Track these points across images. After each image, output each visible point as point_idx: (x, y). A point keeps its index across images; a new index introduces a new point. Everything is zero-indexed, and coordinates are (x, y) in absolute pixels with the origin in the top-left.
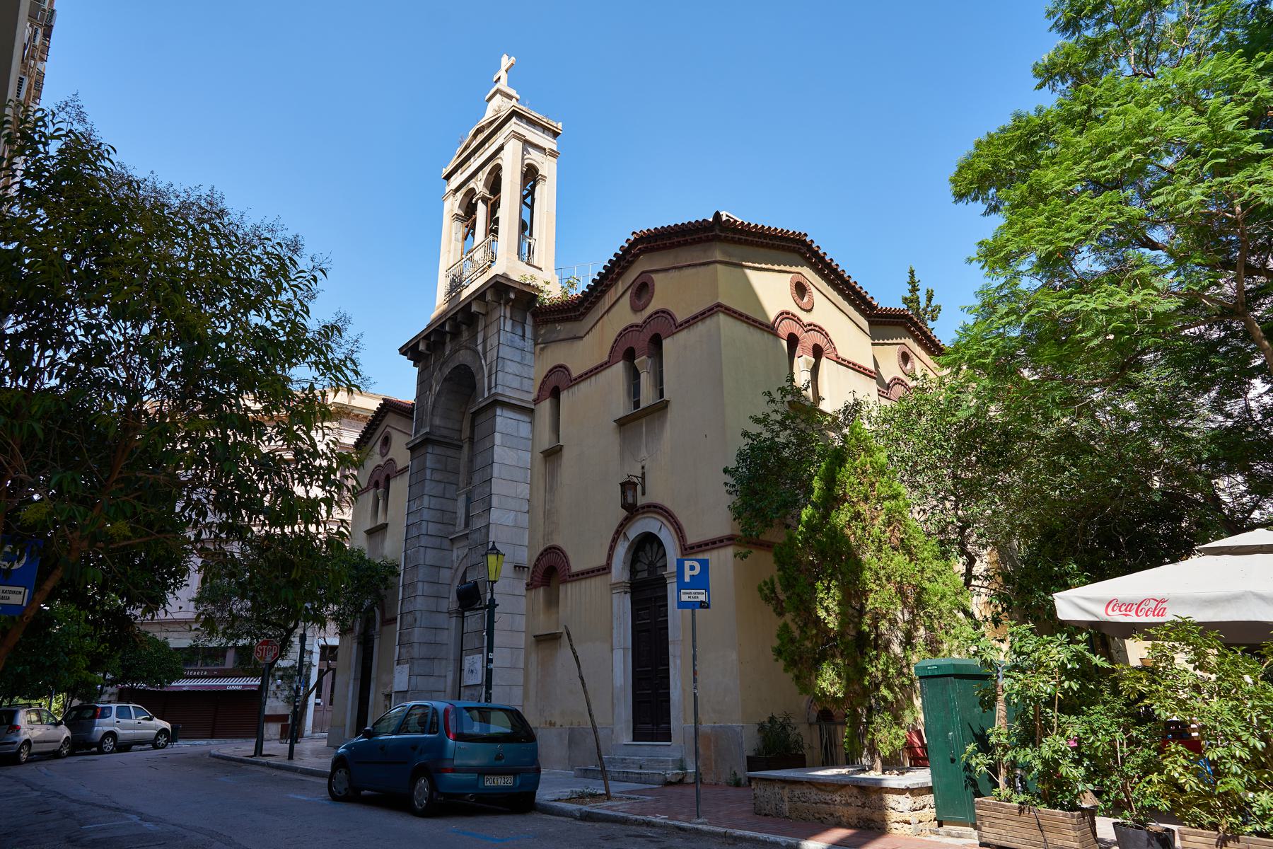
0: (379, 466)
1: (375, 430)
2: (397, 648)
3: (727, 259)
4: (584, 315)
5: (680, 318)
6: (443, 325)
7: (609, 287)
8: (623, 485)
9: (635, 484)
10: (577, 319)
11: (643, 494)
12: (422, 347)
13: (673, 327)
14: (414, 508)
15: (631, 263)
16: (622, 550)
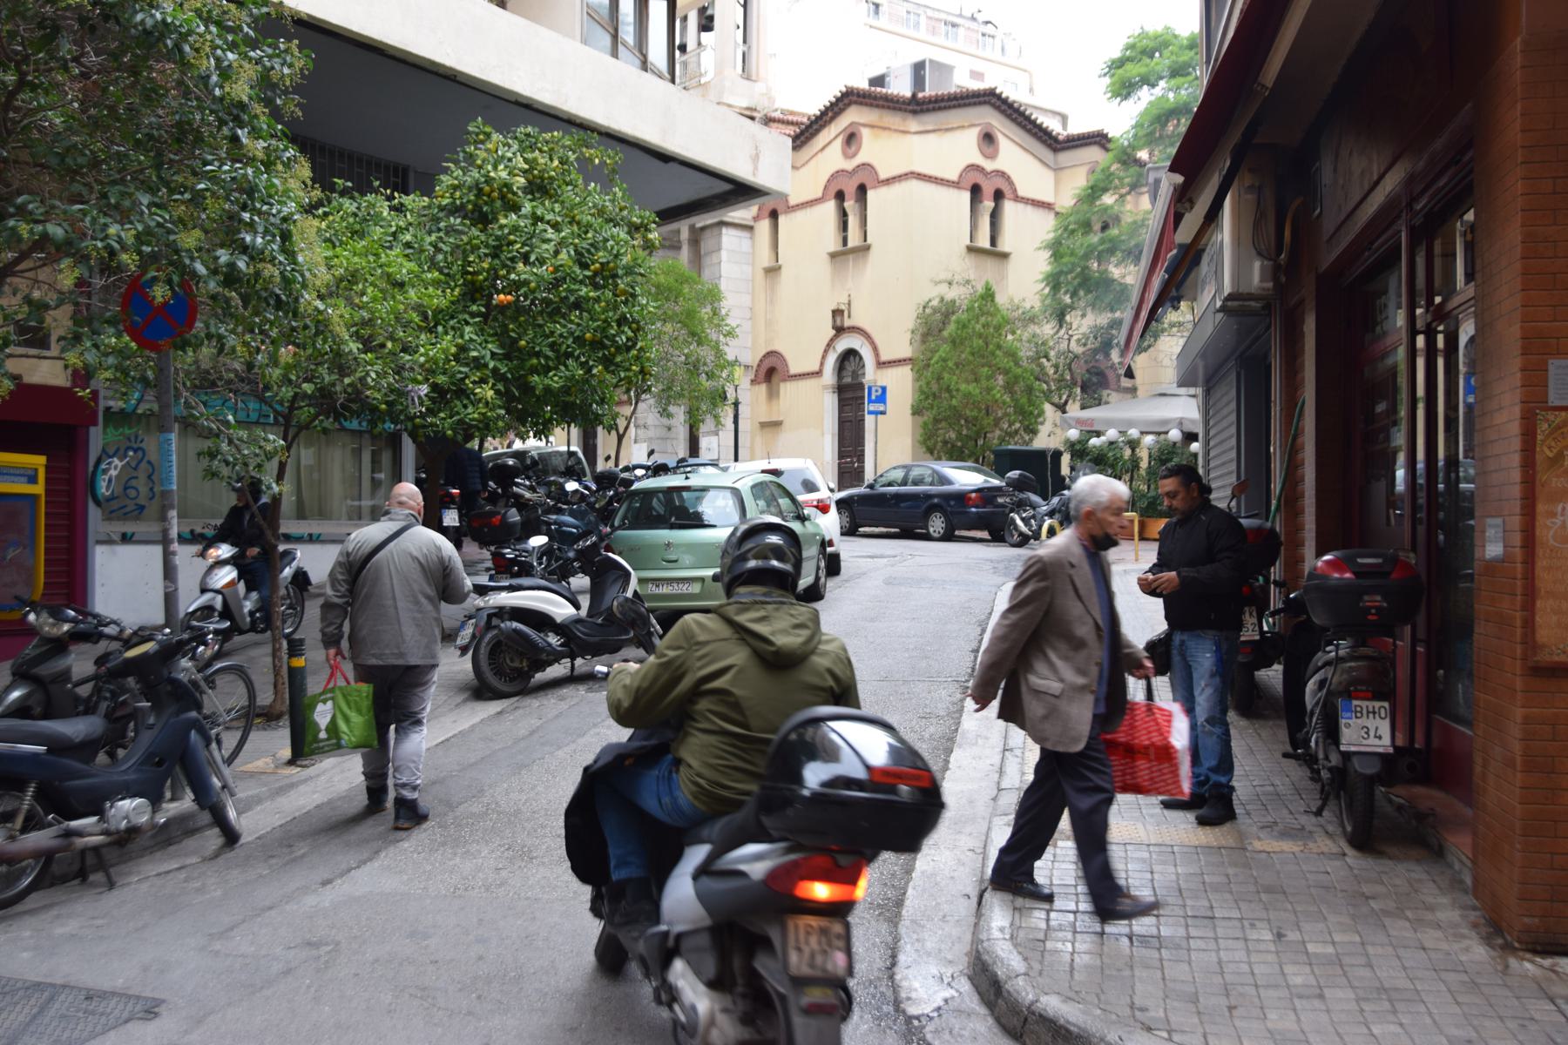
9: (842, 311)
15: (841, 111)
16: (832, 359)
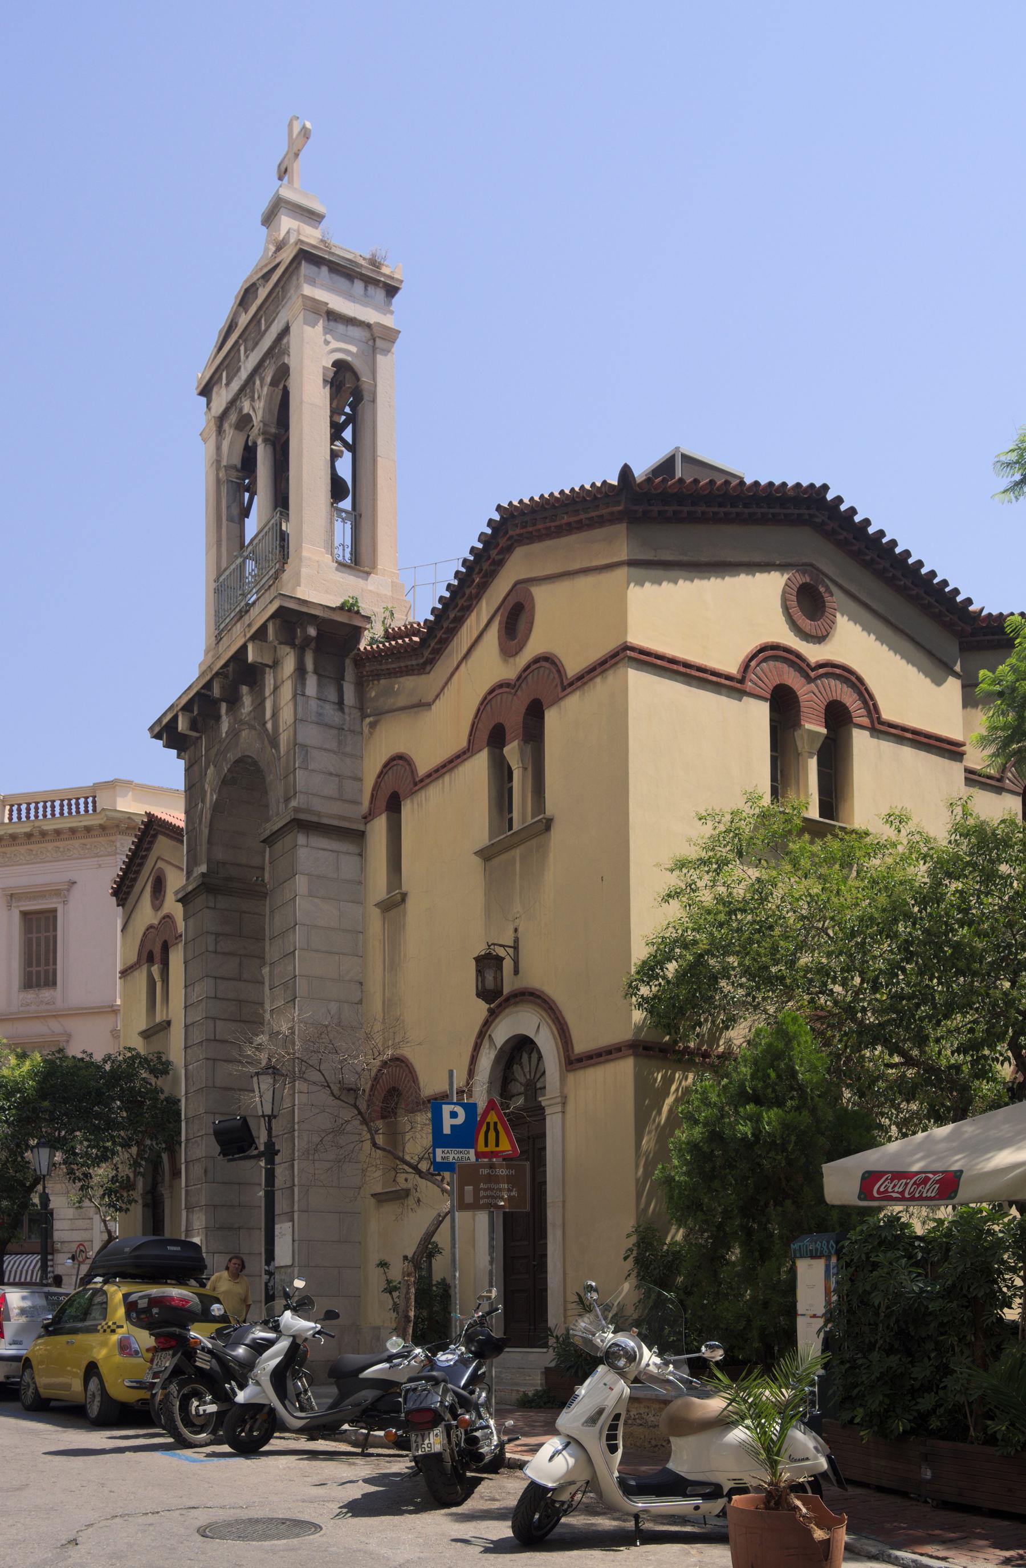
0: (151, 927)
1: (141, 865)
2: (184, 1213)
3: (649, 556)
4: (431, 662)
5: (573, 667)
6: (208, 685)
7: (467, 609)
8: (478, 960)
9: (500, 960)
10: (425, 667)
11: (516, 972)
12: (182, 725)
13: (559, 689)
14: (194, 999)
15: (499, 564)
16: (486, 1060)
